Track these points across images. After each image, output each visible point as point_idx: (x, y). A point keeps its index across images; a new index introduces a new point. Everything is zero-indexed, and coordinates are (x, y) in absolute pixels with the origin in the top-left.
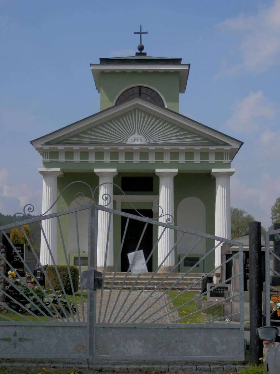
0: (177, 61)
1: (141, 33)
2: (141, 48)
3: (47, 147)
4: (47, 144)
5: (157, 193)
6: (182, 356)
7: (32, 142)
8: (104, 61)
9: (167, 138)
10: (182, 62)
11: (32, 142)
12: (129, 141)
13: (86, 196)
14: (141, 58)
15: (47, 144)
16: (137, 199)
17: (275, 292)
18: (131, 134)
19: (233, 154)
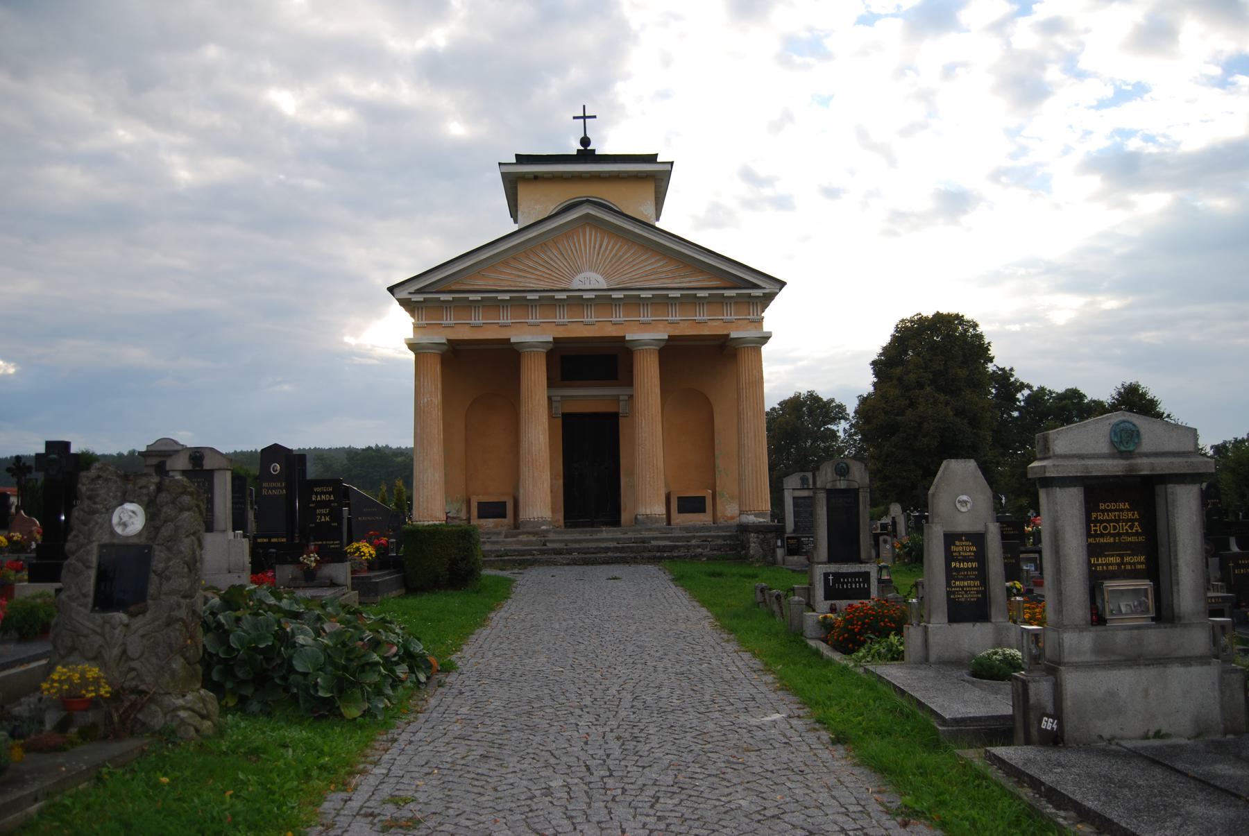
0: (652, 158)
1: (584, 117)
2: (585, 141)
3: (419, 298)
4: (418, 291)
5: (629, 381)
6: (727, 293)
7: (391, 290)
8: (521, 159)
9: (646, 273)
10: (659, 160)
11: (391, 290)
12: (576, 283)
13: (399, 452)
14: (586, 154)
15: (418, 291)
16: (589, 397)
17: (951, 663)
18: (579, 271)
19: (768, 298)
